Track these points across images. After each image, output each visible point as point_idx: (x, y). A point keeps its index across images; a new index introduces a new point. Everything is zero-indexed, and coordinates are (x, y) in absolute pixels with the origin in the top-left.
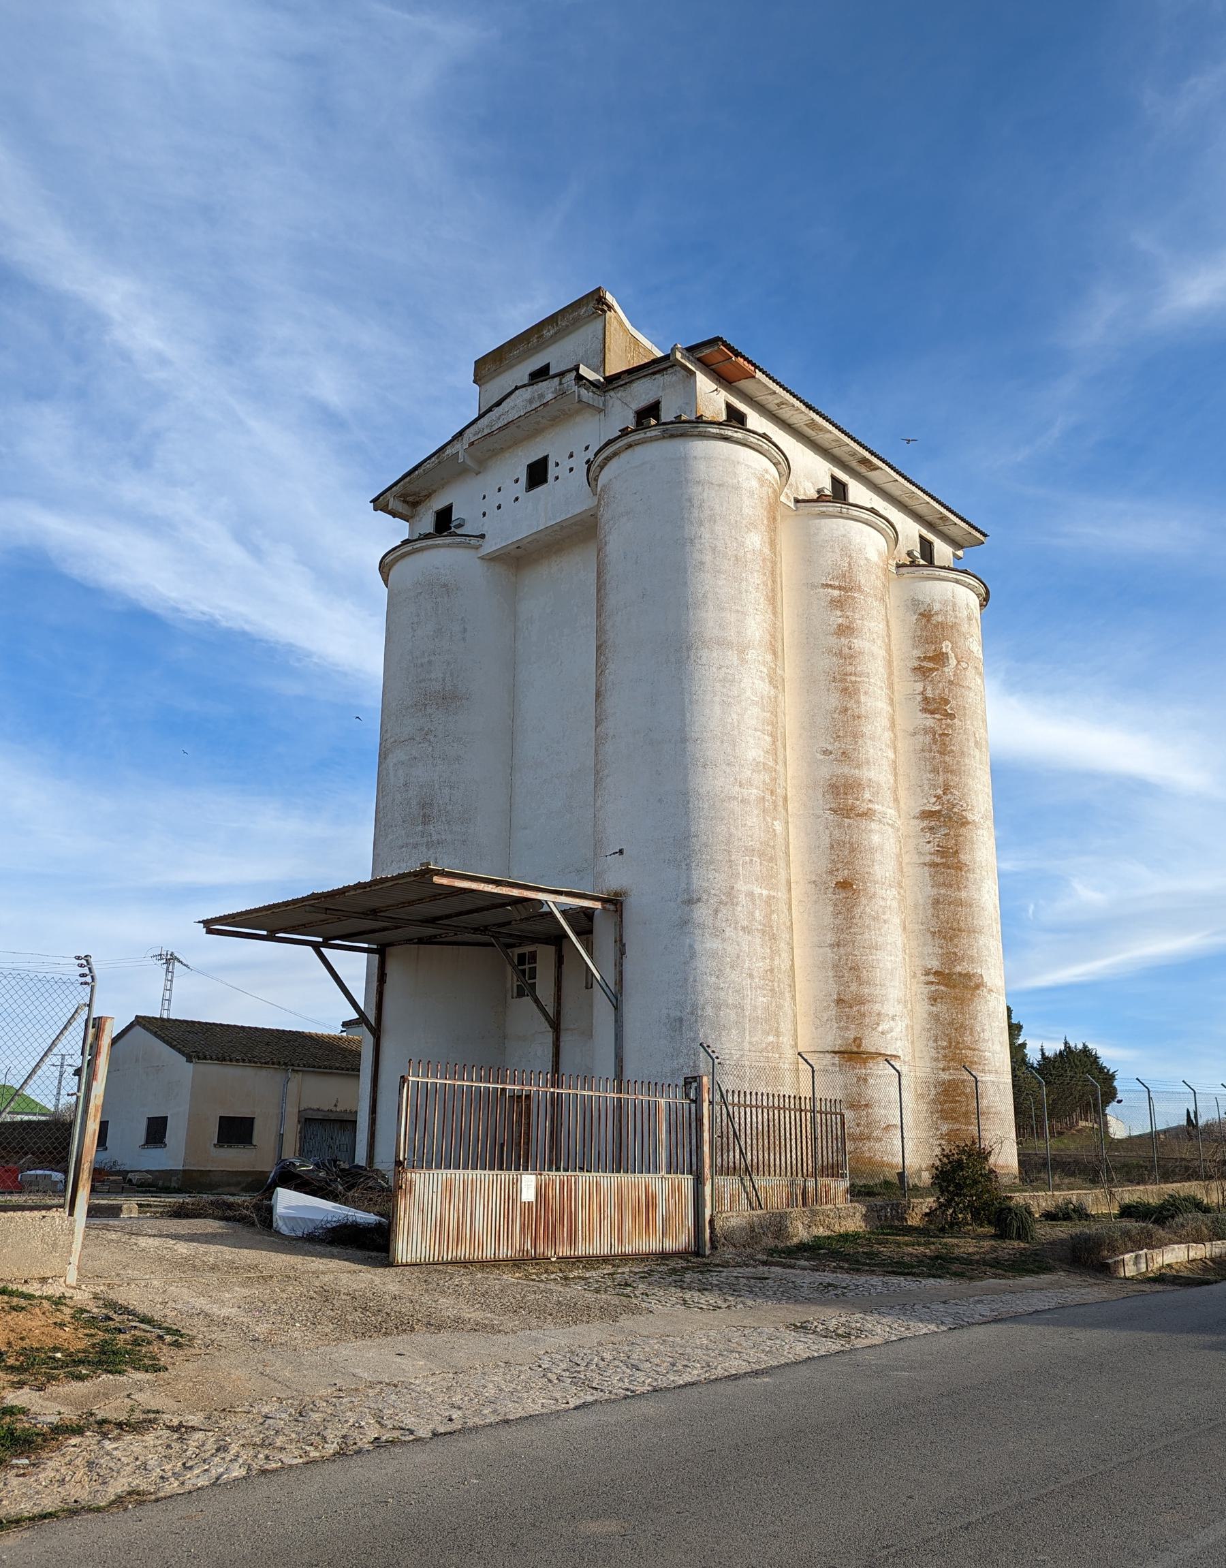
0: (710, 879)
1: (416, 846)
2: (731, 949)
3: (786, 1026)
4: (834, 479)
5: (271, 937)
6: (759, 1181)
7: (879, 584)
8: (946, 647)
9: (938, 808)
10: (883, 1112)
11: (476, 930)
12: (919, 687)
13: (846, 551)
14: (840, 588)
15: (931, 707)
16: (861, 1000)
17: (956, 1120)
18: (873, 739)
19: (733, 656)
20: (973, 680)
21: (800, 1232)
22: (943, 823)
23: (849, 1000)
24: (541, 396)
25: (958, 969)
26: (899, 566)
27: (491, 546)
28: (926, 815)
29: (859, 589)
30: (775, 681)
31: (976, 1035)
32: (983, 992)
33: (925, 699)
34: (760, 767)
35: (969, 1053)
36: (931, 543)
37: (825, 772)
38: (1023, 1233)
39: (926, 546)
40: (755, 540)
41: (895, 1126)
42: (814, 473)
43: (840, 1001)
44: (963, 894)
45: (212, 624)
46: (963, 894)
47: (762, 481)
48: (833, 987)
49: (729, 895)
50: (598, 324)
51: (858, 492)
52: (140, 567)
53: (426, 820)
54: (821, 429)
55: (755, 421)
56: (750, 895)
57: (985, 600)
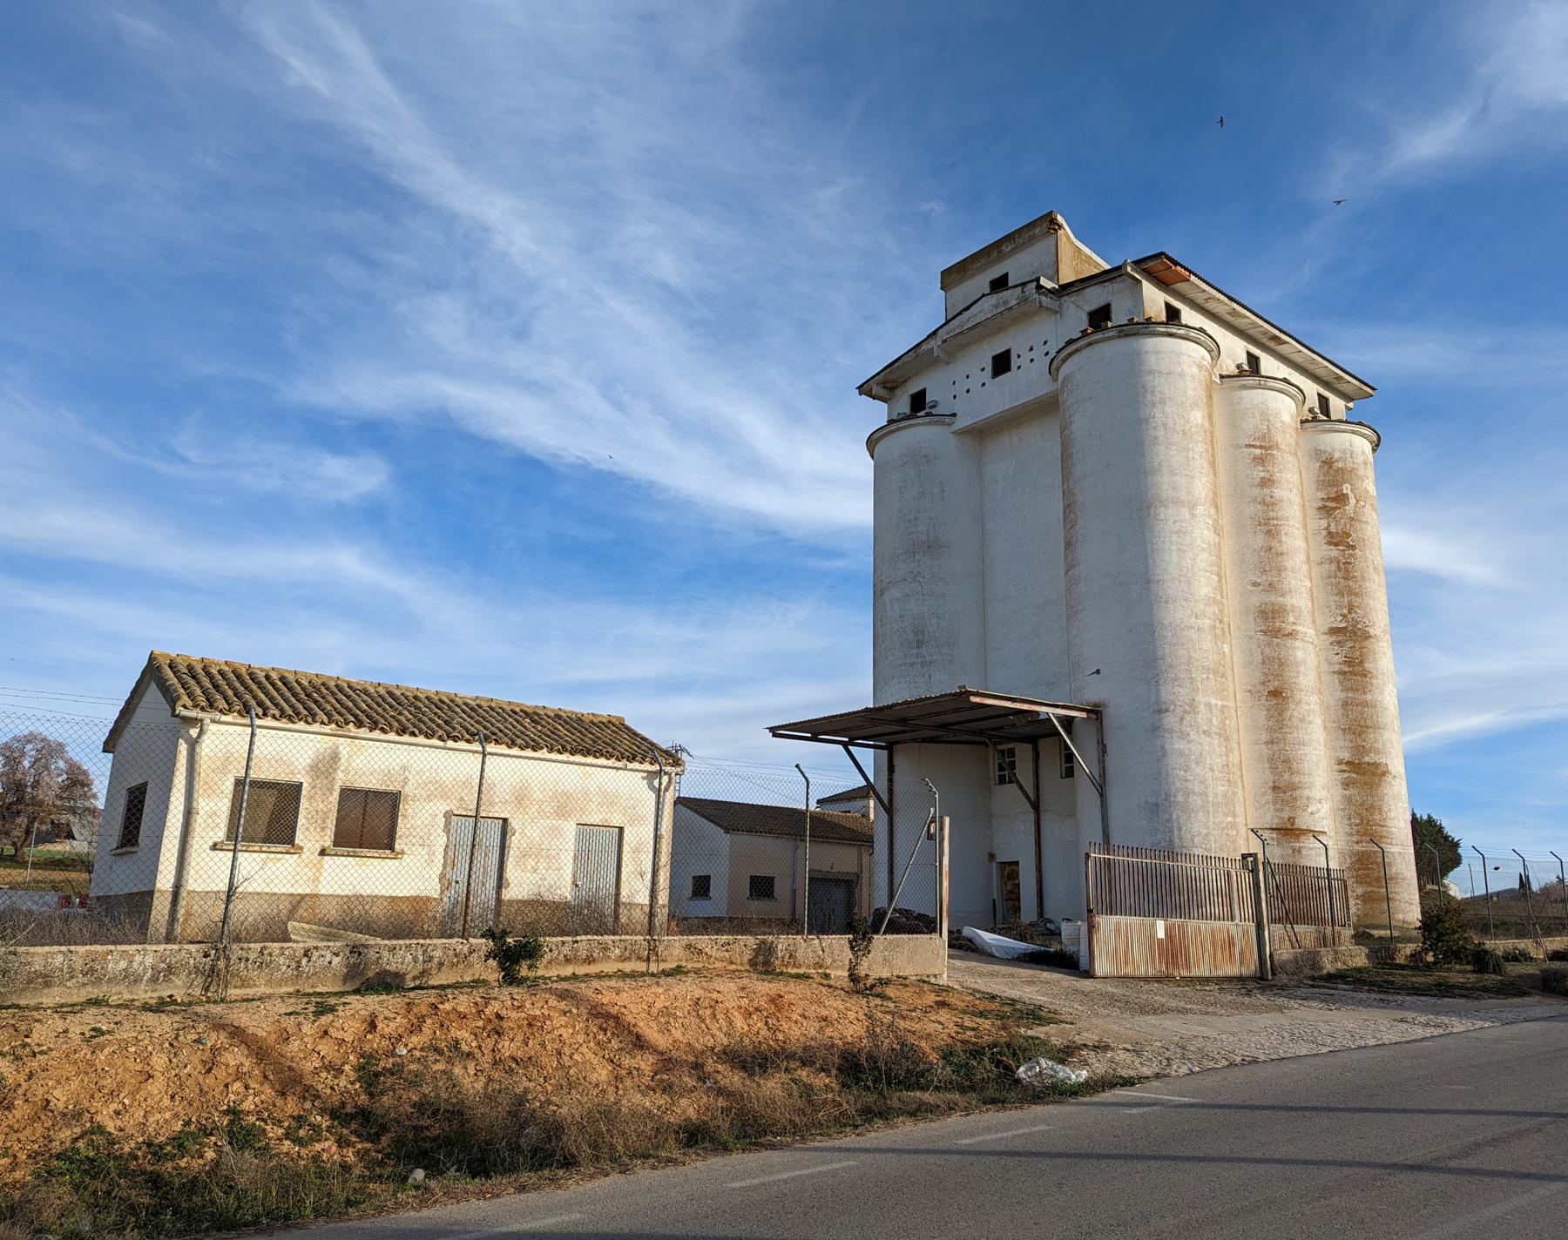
0: (1177, 693)
1: (913, 665)
2: (1195, 748)
3: (1239, 810)
4: (1249, 354)
5: (814, 739)
6: (1297, 928)
7: (1292, 441)
8: (1346, 489)
11: (974, 733)
12: (1324, 523)
13: (1264, 416)
14: (1261, 447)
16: (1293, 787)
17: (1370, 884)
18: (1293, 571)
19: (1185, 513)
20: (1370, 515)
21: (1328, 966)
22: (1350, 639)
23: (1283, 787)
24: (1006, 302)
25: (1367, 759)
26: (1302, 422)
27: (962, 422)
28: (1334, 631)
29: (1277, 447)
30: (1217, 530)
32: (1389, 778)
33: (1330, 533)
34: (1210, 601)
36: (1327, 400)
37: (1255, 600)
38: (1497, 970)
39: (1324, 402)
40: (1198, 416)
42: (1235, 350)
44: (1369, 697)
45: (585, 466)
46: (1369, 697)
47: (1200, 367)
48: (1269, 777)
49: (1191, 705)
50: (1050, 241)
51: (1269, 365)
52: (526, 422)
53: (920, 644)
55: (1189, 316)
56: (1209, 705)
57: (1376, 446)
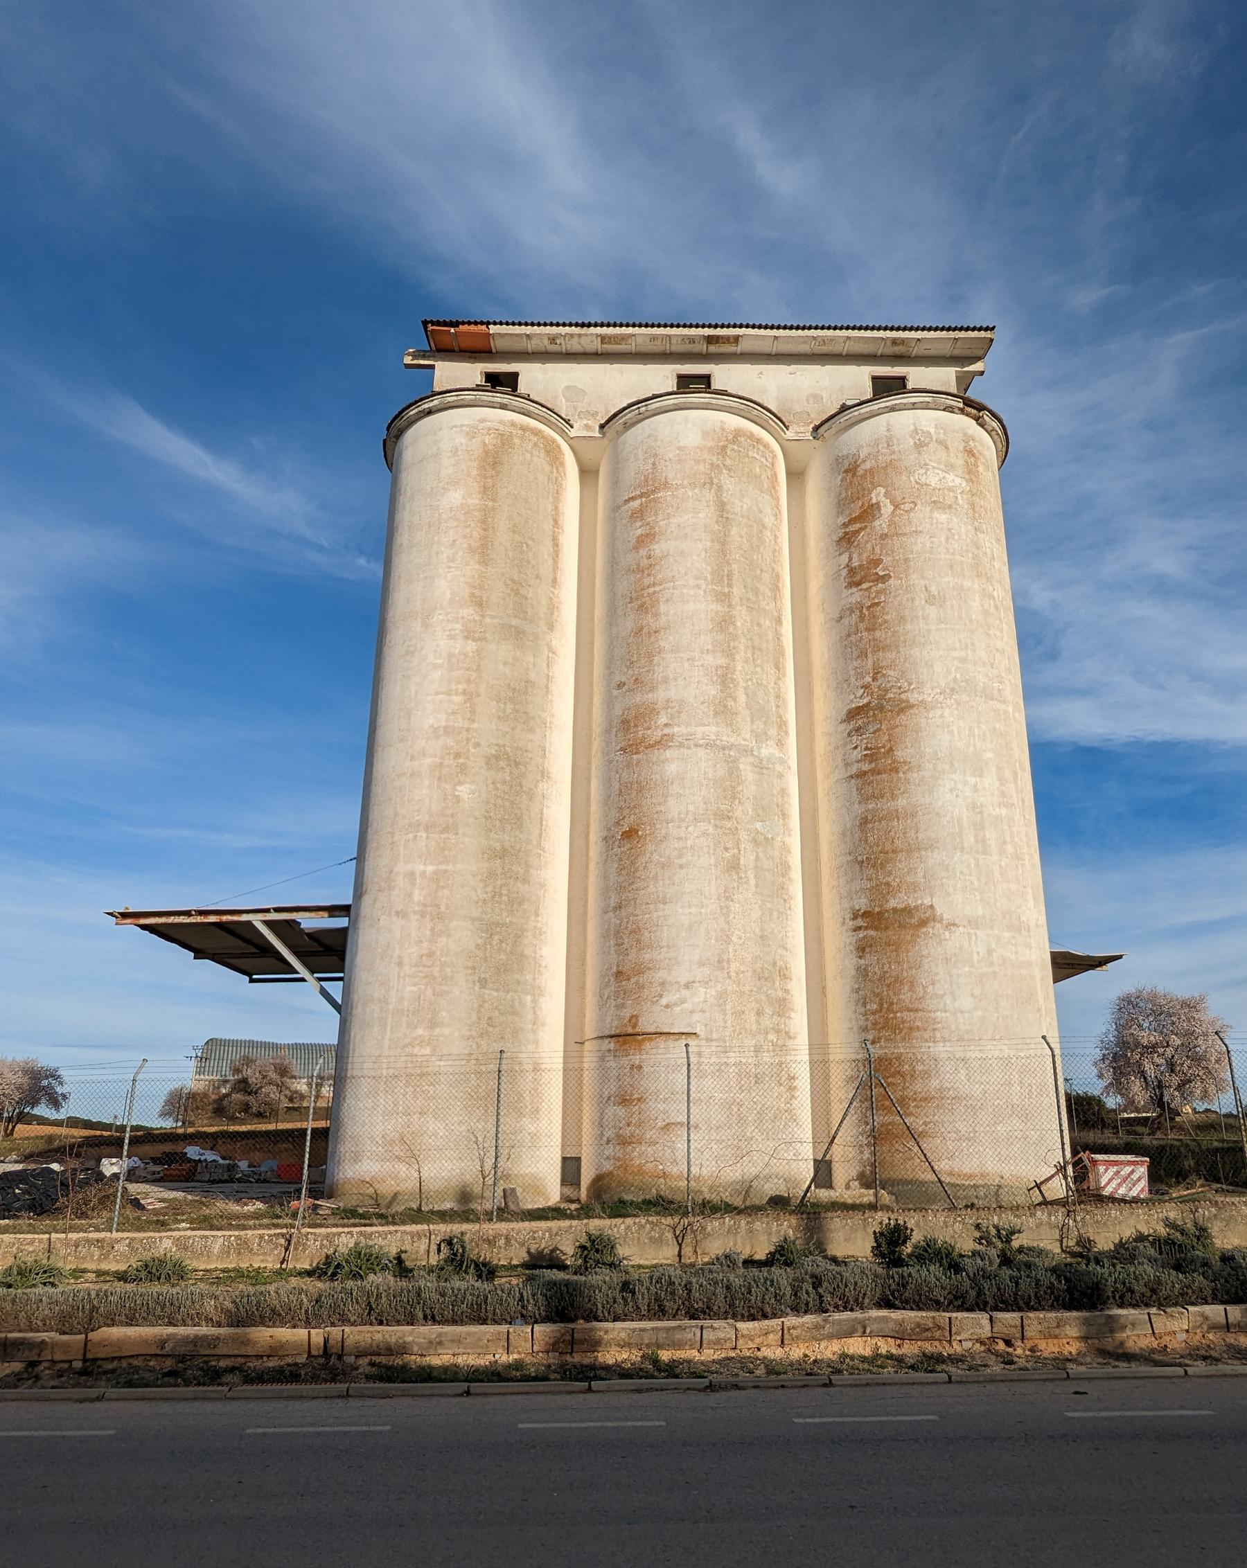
8: (878, 495)
9: (865, 701)
10: (661, 1106)
14: (641, 496)
15: (857, 578)
25: (892, 903)
29: (666, 485)
31: (920, 991)
35: (907, 1016)
41: (681, 1124)
43: (619, 974)
45: (1137, 743)
54: (624, 338)
56: (411, 875)
